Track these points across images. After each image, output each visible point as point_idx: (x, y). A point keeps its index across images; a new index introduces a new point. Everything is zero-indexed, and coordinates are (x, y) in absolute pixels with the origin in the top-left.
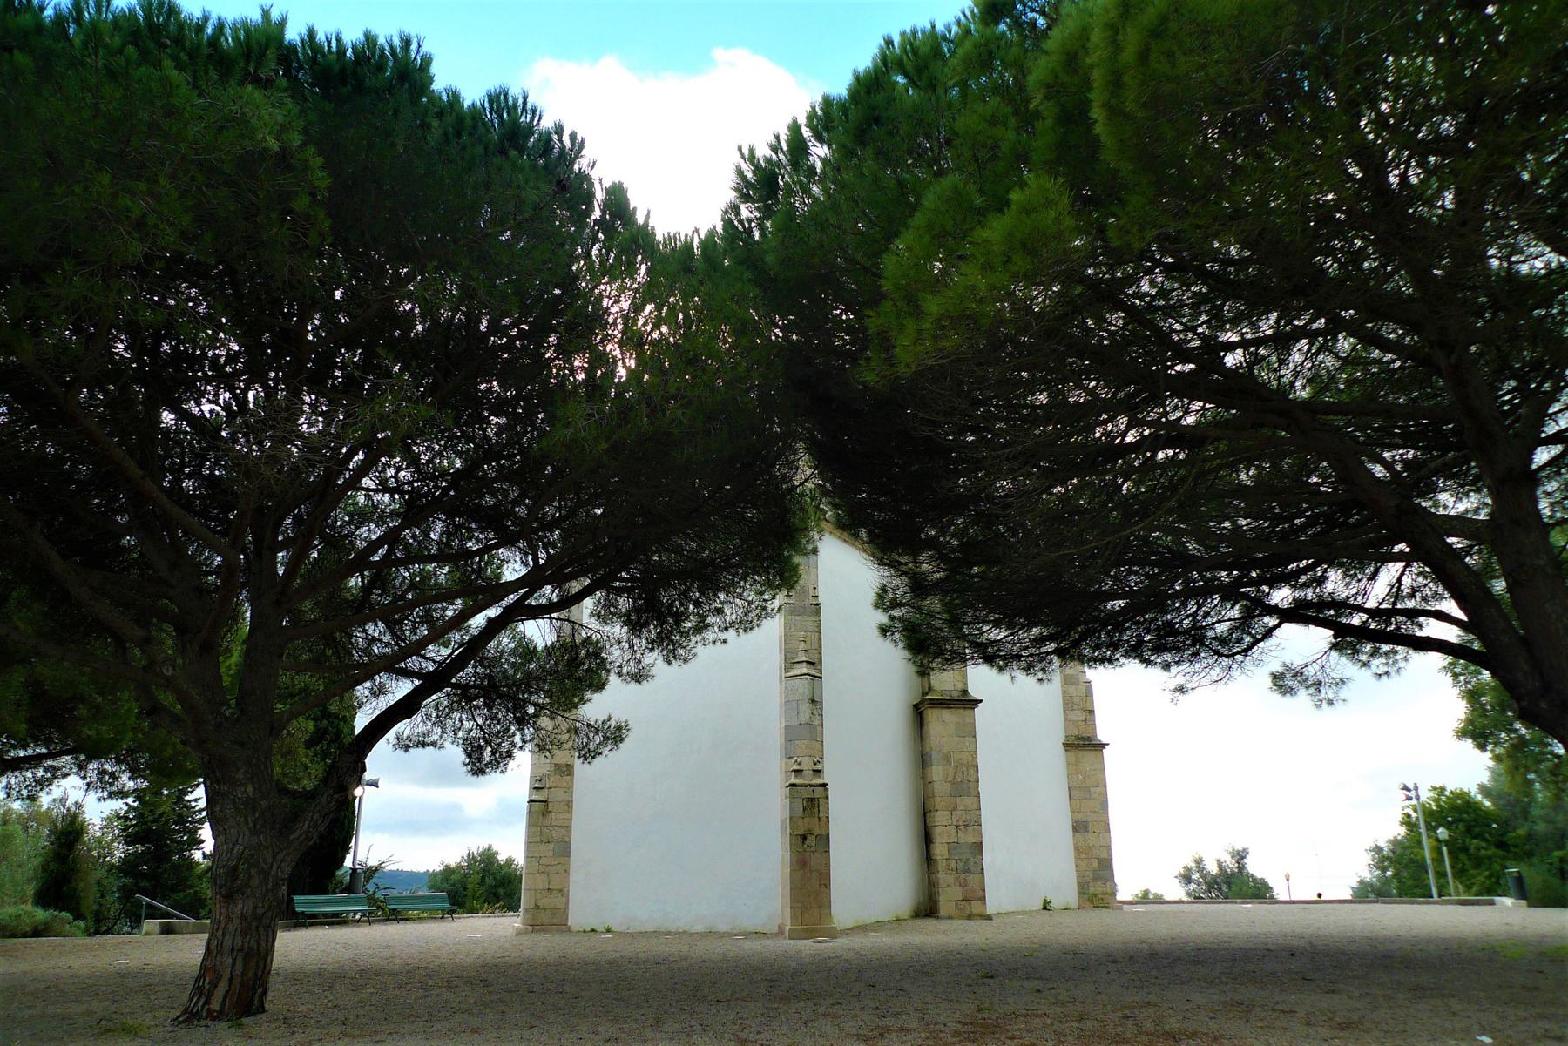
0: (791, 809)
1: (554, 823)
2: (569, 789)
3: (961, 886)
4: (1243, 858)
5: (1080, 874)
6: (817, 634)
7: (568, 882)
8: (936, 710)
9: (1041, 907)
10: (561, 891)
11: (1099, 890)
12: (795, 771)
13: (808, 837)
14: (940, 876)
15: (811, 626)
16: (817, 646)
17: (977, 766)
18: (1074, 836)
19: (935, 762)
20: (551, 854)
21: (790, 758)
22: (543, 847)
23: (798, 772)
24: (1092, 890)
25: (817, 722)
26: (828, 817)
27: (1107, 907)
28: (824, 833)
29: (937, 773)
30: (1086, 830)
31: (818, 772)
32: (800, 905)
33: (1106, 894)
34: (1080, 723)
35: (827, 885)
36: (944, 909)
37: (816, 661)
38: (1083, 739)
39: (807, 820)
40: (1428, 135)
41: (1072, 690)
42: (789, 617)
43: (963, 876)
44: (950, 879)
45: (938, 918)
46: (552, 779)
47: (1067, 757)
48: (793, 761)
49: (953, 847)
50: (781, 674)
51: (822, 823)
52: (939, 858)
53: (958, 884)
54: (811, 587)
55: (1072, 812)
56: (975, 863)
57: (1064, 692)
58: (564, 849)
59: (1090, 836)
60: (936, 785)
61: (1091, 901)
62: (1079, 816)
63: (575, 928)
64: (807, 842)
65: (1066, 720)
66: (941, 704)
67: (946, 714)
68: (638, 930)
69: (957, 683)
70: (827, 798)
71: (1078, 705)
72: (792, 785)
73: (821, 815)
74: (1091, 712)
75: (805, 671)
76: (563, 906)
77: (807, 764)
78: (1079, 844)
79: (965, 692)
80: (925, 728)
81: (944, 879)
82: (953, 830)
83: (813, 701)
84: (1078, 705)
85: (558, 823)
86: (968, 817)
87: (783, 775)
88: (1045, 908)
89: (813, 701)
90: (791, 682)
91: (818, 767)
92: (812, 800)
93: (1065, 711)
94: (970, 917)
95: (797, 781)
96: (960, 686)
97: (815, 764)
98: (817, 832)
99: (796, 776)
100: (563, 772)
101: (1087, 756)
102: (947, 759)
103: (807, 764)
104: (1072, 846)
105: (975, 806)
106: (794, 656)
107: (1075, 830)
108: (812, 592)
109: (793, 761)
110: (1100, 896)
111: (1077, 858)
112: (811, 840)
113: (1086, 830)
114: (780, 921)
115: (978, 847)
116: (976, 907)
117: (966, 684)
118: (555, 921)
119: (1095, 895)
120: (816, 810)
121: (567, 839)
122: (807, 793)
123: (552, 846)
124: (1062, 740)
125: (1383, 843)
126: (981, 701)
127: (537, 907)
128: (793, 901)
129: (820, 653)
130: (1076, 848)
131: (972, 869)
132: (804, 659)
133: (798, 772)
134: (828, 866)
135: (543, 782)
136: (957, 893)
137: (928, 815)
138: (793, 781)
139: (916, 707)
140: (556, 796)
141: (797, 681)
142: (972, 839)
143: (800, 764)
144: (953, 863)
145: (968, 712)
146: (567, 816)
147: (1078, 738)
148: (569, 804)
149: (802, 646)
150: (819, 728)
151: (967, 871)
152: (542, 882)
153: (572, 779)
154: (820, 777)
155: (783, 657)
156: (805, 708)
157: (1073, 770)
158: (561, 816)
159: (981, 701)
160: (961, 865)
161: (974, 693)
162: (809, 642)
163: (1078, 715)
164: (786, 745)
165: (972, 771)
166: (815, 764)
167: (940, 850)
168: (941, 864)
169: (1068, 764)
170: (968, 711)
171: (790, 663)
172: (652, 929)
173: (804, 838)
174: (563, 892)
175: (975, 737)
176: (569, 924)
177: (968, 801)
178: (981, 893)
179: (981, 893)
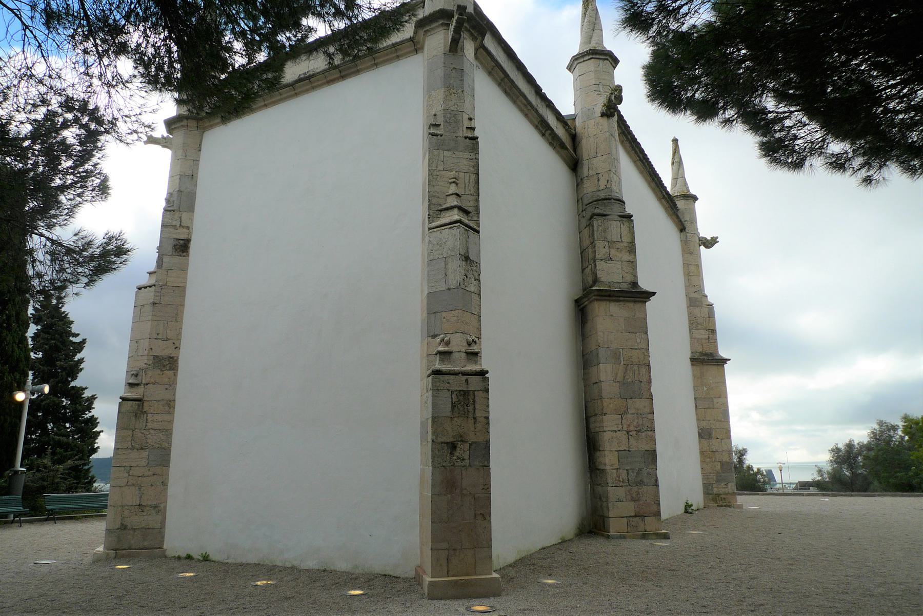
0: (434, 406)
1: (150, 425)
2: (171, 385)
3: (633, 500)
4: (742, 455)
5: (705, 476)
6: (473, 176)
7: (166, 496)
8: (604, 303)
9: (683, 510)
10: (156, 507)
11: (722, 491)
12: (440, 353)
13: (460, 445)
14: (609, 488)
15: (465, 165)
16: (472, 190)
17: (649, 365)
18: (700, 441)
19: (602, 360)
20: (144, 462)
21: (434, 336)
22: (134, 454)
23: (445, 355)
24: (715, 491)
25: (472, 288)
26: (487, 418)
27: (729, 506)
28: (481, 439)
29: (605, 372)
30: (710, 437)
31: (474, 355)
32: (445, 545)
33: (728, 494)
34: (704, 341)
35: (486, 515)
36: (615, 526)
37: (470, 209)
38: (706, 354)
39: (457, 421)
40: (781, 70)
41: (697, 311)
42: (436, 152)
43: (635, 489)
44: (621, 492)
45: (608, 537)
46: (150, 373)
47: (693, 370)
48: (438, 340)
49: (624, 455)
50: (423, 224)
51: (479, 425)
52: (608, 467)
53: (629, 497)
54: (466, 117)
55: (698, 420)
56: (649, 474)
57: (690, 314)
58: (162, 457)
59: (714, 441)
60: (604, 386)
61: (714, 500)
62: (704, 424)
63: (170, 553)
64: (457, 453)
65: (691, 338)
66: (609, 296)
67: (614, 308)
68: (239, 561)
69: (625, 275)
70: (487, 391)
71: (701, 325)
72: (437, 373)
73: (478, 414)
74: (713, 331)
75: (456, 217)
76: (159, 526)
77: (458, 344)
78: (705, 449)
79: (635, 284)
80: (589, 325)
81: (614, 493)
82: (622, 436)
83: (467, 258)
84: (701, 325)
85: (155, 426)
86: (641, 422)
87: (425, 361)
88: (686, 512)
89: (467, 258)
90: (437, 234)
91: (475, 348)
92: (465, 393)
93: (690, 330)
94: (644, 536)
95: (443, 367)
96: (629, 278)
97: (469, 344)
98: (472, 438)
99: (442, 361)
100: (164, 366)
101: (712, 370)
102: (616, 356)
103: (458, 344)
104: (698, 451)
105: (647, 410)
106: (442, 202)
107: (701, 436)
108: (466, 124)
109: (438, 340)
110: (723, 496)
111: (703, 462)
112: (463, 450)
113: (710, 437)
114: (418, 562)
115: (652, 456)
116: (650, 524)
117: (636, 276)
118: (146, 544)
119: (719, 495)
120: (471, 408)
121: (165, 445)
122: (457, 383)
123: (145, 454)
124: (689, 355)
125: (841, 446)
126: (654, 294)
127: (124, 527)
128: (435, 538)
129: (477, 201)
130: (702, 453)
131: (645, 480)
132: (455, 203)
133: (445, 355)
134: (487, 488)
135: (139, 377)
136: (628, 508)
137: (592, 420)
138: (438, 367)
139: (577, 302)
140: (154, 393)
141: (446, 232)
142: (644, 447)
143: (448, 343)
144: (624, 475)
145: (638, 306)
146: (166, 417)
147: (702, 354)
148: (170, 405)
149: (453, 189)
150: (475, 297)
151: (640, 483)
152: (131, 497)
153: (175, 375)
154: (476, 363)
155: (427, 204)
156: (456, 269)
157: (699, 382)
158: (159, 417)
159: (654, 294)
160: (632, 476)
161: (645, 284)
162: (461, 185)
163: (702, 334)
164: (429, 318)
165: (644, 370)
166: (469, 344)
167: (608, 459)
168: (611, 475)
169: (694, 376)
170: (638, 305)
171: (435, 210)
172: (255, 561)
173: (453, 447)
174: (159, 509)
175: (646, 333)
176: (165, 547)
177: (640, 404)
178: (655, 508)
179: (655, 508)
